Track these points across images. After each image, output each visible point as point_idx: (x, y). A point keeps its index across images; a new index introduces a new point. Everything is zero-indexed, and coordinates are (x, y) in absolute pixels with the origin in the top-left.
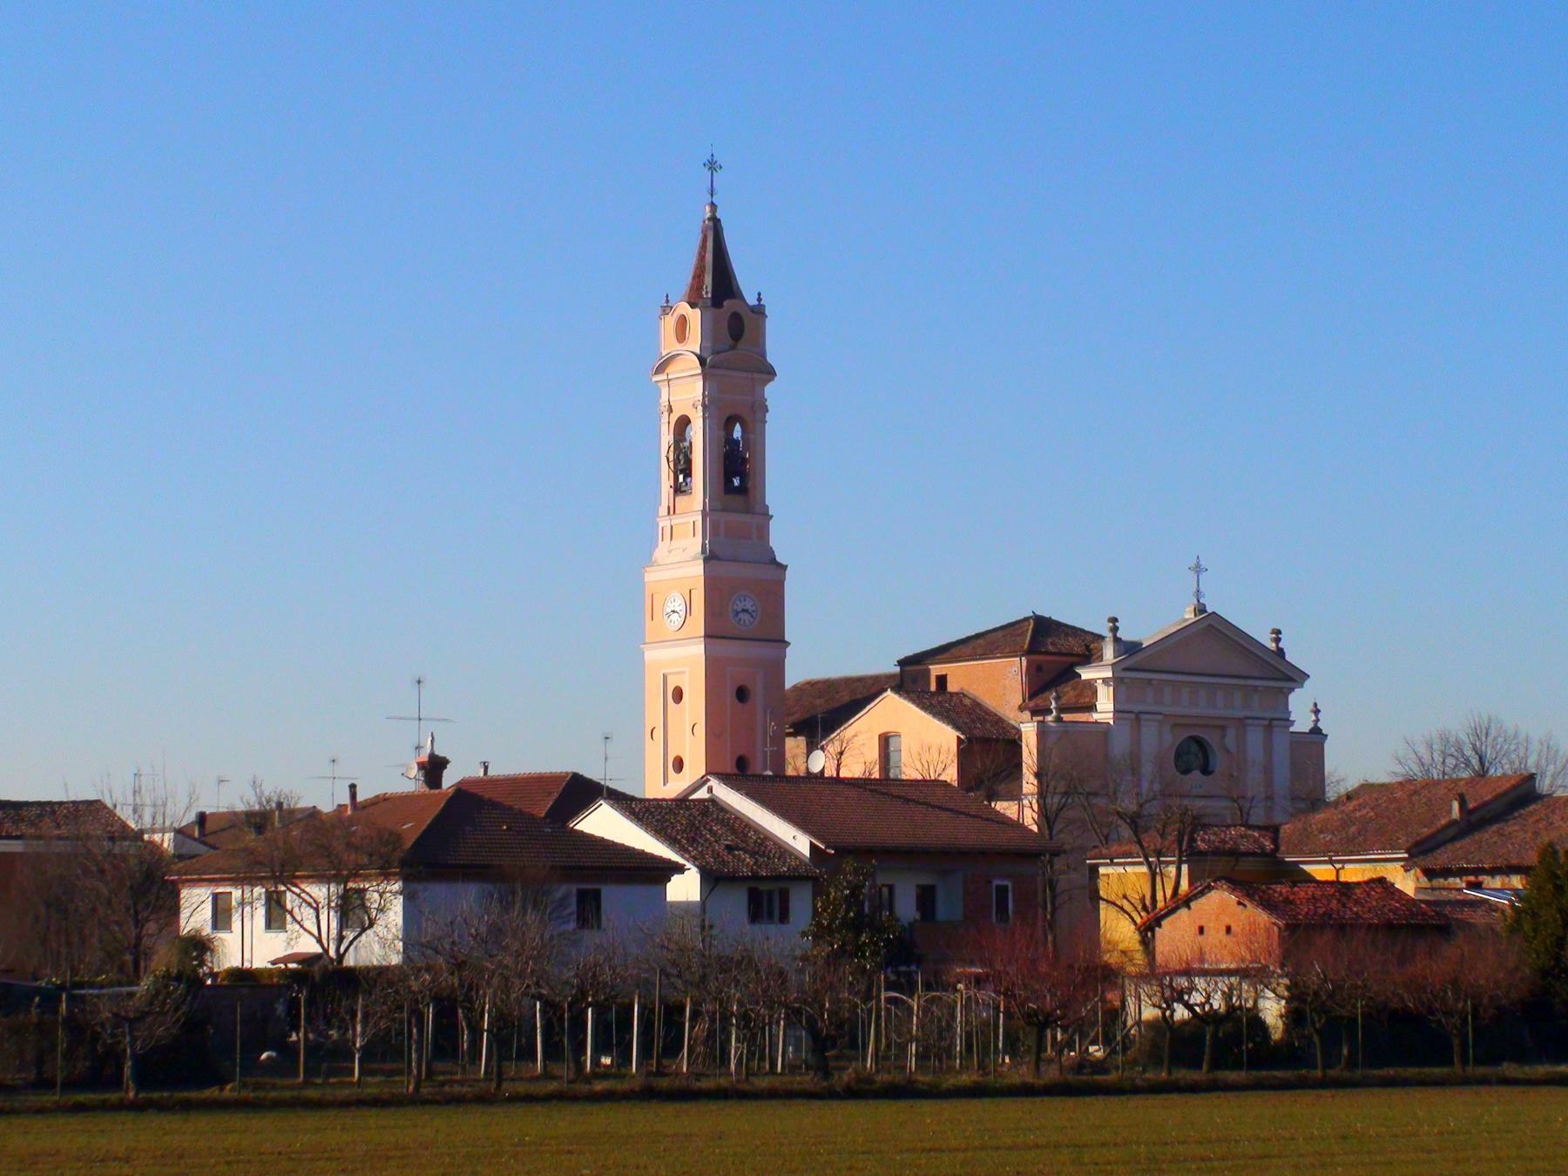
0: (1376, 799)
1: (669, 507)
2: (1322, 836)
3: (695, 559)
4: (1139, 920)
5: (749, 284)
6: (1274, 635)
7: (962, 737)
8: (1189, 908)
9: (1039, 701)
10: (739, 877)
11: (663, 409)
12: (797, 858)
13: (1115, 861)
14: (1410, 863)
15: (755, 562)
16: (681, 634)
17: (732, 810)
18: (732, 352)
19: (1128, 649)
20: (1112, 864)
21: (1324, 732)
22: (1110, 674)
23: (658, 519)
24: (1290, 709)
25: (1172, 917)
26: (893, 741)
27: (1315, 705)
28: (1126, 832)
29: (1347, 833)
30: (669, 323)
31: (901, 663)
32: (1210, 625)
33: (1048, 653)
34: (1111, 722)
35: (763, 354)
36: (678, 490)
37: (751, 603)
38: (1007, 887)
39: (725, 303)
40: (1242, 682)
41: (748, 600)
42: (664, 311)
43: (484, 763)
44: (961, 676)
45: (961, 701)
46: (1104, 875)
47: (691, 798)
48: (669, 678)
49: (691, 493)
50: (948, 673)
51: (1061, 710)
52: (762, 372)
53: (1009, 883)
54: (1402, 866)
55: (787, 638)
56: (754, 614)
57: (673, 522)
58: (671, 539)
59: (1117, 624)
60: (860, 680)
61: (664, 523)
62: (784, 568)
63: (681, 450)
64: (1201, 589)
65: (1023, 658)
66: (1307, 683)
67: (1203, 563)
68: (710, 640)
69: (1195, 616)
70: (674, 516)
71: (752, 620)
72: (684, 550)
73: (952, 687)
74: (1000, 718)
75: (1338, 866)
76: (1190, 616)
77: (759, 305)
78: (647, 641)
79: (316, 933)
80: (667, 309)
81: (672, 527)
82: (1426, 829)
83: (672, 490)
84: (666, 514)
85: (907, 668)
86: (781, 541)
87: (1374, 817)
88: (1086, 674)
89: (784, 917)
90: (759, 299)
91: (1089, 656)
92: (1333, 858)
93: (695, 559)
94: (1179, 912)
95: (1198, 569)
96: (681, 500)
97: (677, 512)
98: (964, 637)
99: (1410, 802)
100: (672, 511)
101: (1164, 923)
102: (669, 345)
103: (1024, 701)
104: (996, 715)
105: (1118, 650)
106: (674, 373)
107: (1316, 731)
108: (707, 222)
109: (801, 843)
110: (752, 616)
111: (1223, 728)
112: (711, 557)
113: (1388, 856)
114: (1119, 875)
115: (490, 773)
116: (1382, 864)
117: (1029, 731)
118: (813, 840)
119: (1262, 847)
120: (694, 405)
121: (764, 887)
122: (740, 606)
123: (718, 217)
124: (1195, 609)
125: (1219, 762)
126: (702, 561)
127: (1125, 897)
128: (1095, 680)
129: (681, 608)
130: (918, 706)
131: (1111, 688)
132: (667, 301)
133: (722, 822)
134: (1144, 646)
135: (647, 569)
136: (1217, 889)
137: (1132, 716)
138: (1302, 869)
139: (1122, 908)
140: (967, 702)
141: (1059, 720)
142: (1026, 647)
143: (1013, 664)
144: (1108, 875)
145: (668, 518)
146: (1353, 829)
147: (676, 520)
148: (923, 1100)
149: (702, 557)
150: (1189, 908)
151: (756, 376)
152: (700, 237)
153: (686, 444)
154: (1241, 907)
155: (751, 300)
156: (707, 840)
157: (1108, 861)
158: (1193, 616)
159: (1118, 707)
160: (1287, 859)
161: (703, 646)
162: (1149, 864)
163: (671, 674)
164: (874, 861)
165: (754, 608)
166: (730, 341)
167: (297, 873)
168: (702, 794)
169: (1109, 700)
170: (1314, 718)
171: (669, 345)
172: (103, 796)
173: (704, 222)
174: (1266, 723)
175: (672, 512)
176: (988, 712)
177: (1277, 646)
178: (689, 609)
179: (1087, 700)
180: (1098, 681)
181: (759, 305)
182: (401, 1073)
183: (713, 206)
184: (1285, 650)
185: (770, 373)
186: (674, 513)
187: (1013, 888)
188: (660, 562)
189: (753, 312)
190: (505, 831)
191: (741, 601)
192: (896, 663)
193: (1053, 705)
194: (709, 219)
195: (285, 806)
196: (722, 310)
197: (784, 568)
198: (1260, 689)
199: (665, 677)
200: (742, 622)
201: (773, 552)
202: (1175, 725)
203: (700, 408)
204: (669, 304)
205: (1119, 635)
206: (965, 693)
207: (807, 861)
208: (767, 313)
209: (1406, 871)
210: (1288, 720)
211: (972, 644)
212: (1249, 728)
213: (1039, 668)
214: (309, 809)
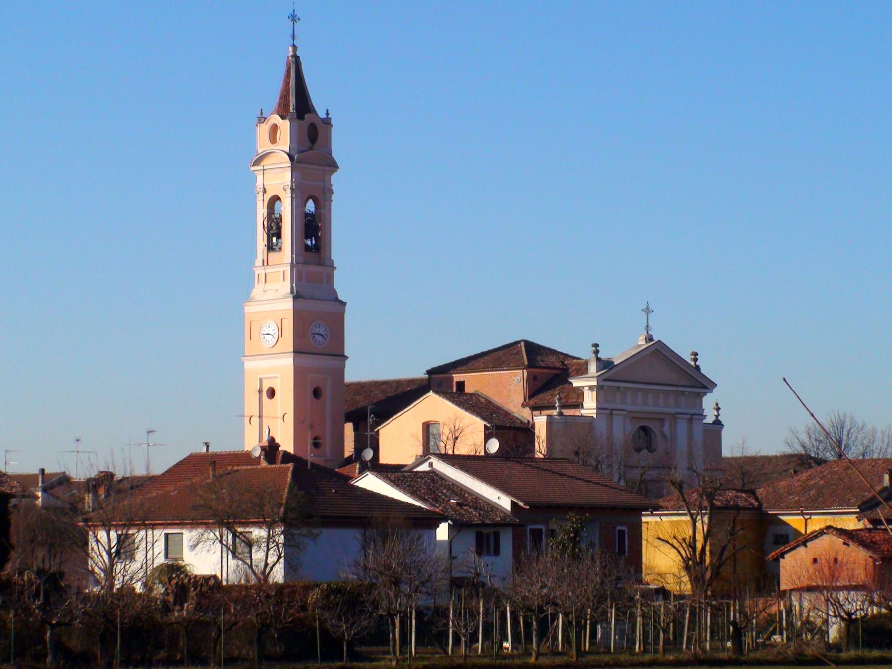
0: (821, 472)
1: (263, 261)
2: (791, 497)
3: (285, 297)
4: (684, 554)
5: (320, 103)
6: (693, 357)
7: (488, 425)
8: (806, 546)
9: (538, 400)
10: (474, 524)
11: (258, 190)
12: (502, 512)
13: (654, 513)
14: (862, 515)
15: (330, 301)
16: (274, 351)
17: (449, 479)
18: (311, 152)
19: (605, 365)
20: (652, 515)
21: (722, 423)
22: (594, 383)
23: (254, 269)
24: (703, 407)
25: (793, 552)
26: (433, 430)
27: (717, 404)
28: (676, 493)
29: (809, 494)
30: (264, 129)
31: (429, 372)
32: (657, 350)
33: (540, 367)
34: (595, 416)
35: (330, 154)
36: (270, 248)
37: (323, 329)
38: (624, 531)
39: (305, 117)
40: (675, 389)
41: (321, 326)
42: (259, 120)
43: (206, 443)
44: (474, 382)
45: (478, 399)
46: (645, 522)
47: (415, 470)
48: (264, 381)
49: (280, 249)
50: (466, 380)
51: (563, 407)
52: (330, 166)
53: (624, 528)
54: (857, 518)
55: (346, 354)
56: (325, 337)
57: (267, 271)
58: (265, 282)
59: (598, 348)
60: (399, 383)
61: (260, 271)
62: (344, 304)
63: (273, 221)
64: (650, 324)
65: (525, 371)
66: (715, 390)
67: (651, 307)
68: (296, 354)
69: (646, 343)
70: (267, 267)
71: (324, 341)
72: (276, 291)
73: (468, 389)
74: (507, 412)
75: (807, 517)
76: (642, 343)
77: (327, 118)
78: (246, 354)
79: (249, 563)
80: (262, 119)
81: (265, 274)
82: (867, 493)
83: (266, 248)
84: (261, 264)
85: (434, 376)
86: (342, 285)
87: (824, 484)
88: (576, 383)
89: (497, 552)
90: (327, 114)
91: (582, 369)
92: (804, 512)
93: (285, 297)
94: (798, 549)
95: (648, 311)
96: (272, 255)
97: (269, 264)
98: (473, 354)
99: (847, 474)
100: (266, 263)
101: (787, 556)
102: (263, 144)
103: (525, 400)
104: (503, 410)
105: (599, 367)
106: (267, 165)
107: (717, 423)
108: (290, 58)
109: (504, 502)
110: (324, 338)
111: (662, 420)
112: (297, 297)
113: (844, 511)
114: (656, 522)
115: (211, 450)
116: (840, 516)
117: (540, 422)
118: (514, 500)
119: (752, 504)
120: (284, 188)
121: (485, 531)
122: (317, 331)
123: (298, 54)
124: (646, 339)
125: (659, 444)
126: (291, 299)
127: (675, 537)
128: (583, 387)
129: (274, 331)
130: (453, 403)
131: (594, 393)
132: (262, 114)
133: (445, 487)
134: (616, 363)
135: (247, 304)
136: (828, 534)
137: (608, 412)
138: (780, 519)
139: (672, 545)
140: (482, 400)
141: (561, 414)
142: (526, 363)
143: (515, 375)
144: (647, 523)
145: (263, 267)
146: (813, 492)
147: (269, 270)
148: (884, 666)
149: (291, 296)
150: (806, 546)
151: (327, 168)
152: (285, 69)
153: (278, 216)
154: (845, 546)
155: (322, 115)
156: (443, 499)
157: (649, 513)
158: (644, 343)
159: (599, 406)
160: (769, 512)
161: (292, 359)
162: (691, 515)
163: (265, 378)
164: (587, 515)
165: (325, 332)
166: (309, 144)
167: (146, 522)
168: (424, 468)
169: (592, 401)
170: (716, 413)
171: (263, 144)
172: (115, 470)
173: (288, 58)
174: (689, 416)
175: (265, 264)
176: (498, 408)
177: (695, 363)
178: (281, 333)
179: (574, 401)
180: (585, 388)
181: (327, 118)
182: (389, 653)
183: (295, 47)
184: (700, 367)
185: (334, 166)
186: (267, 264)
187: (628, 531)
188: (257, 298)
189: (324, 123)
190: (334, 493)
191: (317, 328)
192: (425, 372)
193: (557, 404)
194: (292, 56)
195: (46, 472)
196: (305, 121)
197: (344, 304)
198: (686, 393)
199: (261, 380)
200: (317, 343)
201: (336, 293)
202: (634, 418)
203: (289, 191)
204: (263, 116)
205: (599, 356)
206: (479, 394)
207: (510, 514)
208: (332, 123)
209: (859, 521)
210: (702, 415)
211: (481, 360)
212: (678, 420)
213: (535, 378)
214: (61, 473)
